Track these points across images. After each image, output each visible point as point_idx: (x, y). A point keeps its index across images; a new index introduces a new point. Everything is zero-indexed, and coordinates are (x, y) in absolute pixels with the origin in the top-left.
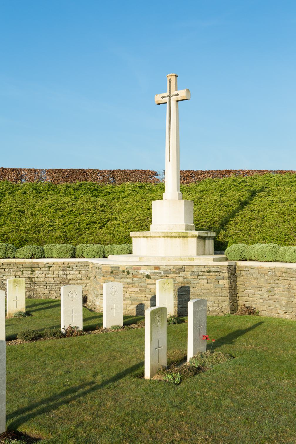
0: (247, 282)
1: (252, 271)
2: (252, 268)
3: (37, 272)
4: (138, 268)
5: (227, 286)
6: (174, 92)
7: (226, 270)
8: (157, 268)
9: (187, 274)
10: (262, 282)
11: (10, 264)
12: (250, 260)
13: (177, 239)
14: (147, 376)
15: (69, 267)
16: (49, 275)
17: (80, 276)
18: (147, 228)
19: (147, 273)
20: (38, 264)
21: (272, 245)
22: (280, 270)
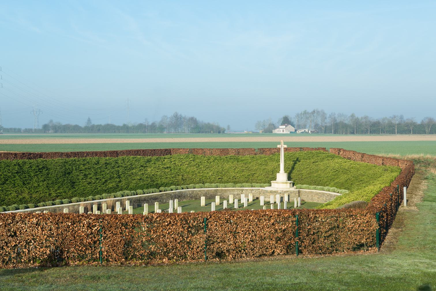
0: (302, 194)
1: (304, 192)
2: (303, 191)
3: (243, 191)
4: (278, 191)
5: (298, 195)
6: (283, 145)
7: (297, 191)
8: (282, 191)
9: (289, 192)
10: (306, 194)
11: (236, 189)
12: (302, 189)
13: (281, 184)
14: (295, 207)
15: (253, 190)
16: (58, 191)
17: (256, 192)
18: (275, 179)
19: (280, 192)
20: (244, 189)
21: (308, 185)
22: (310, 191)
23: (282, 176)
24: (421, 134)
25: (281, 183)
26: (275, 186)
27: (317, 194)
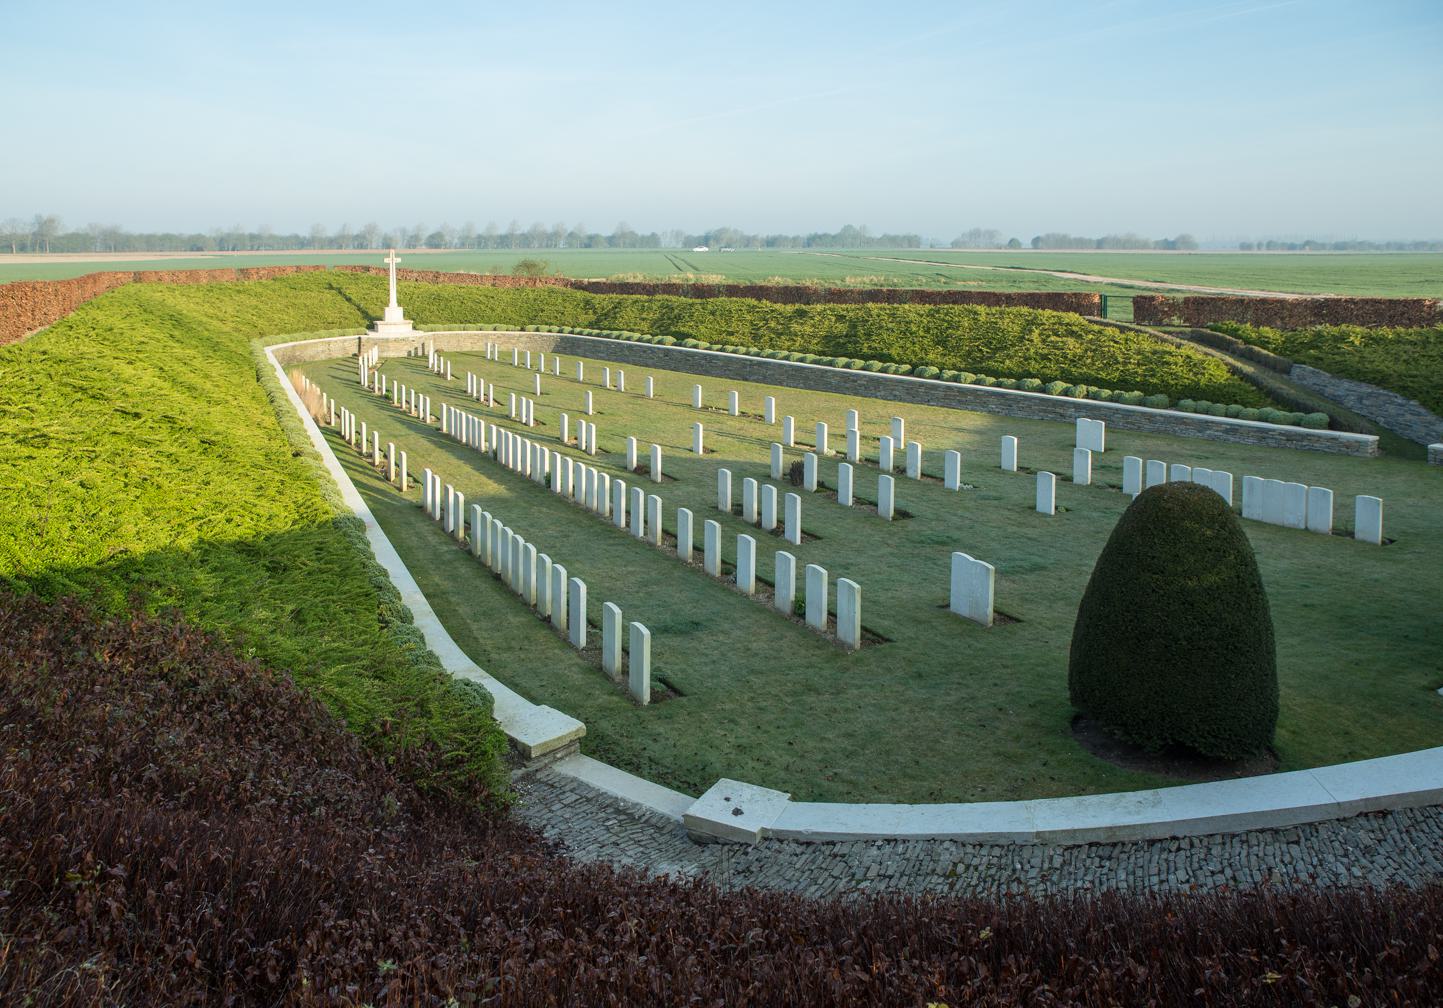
15: (345, 341)
23: (394, 312)
24: (62, 252)
25: (395, 325)
26: (383, 330)
27: (470, 337)
